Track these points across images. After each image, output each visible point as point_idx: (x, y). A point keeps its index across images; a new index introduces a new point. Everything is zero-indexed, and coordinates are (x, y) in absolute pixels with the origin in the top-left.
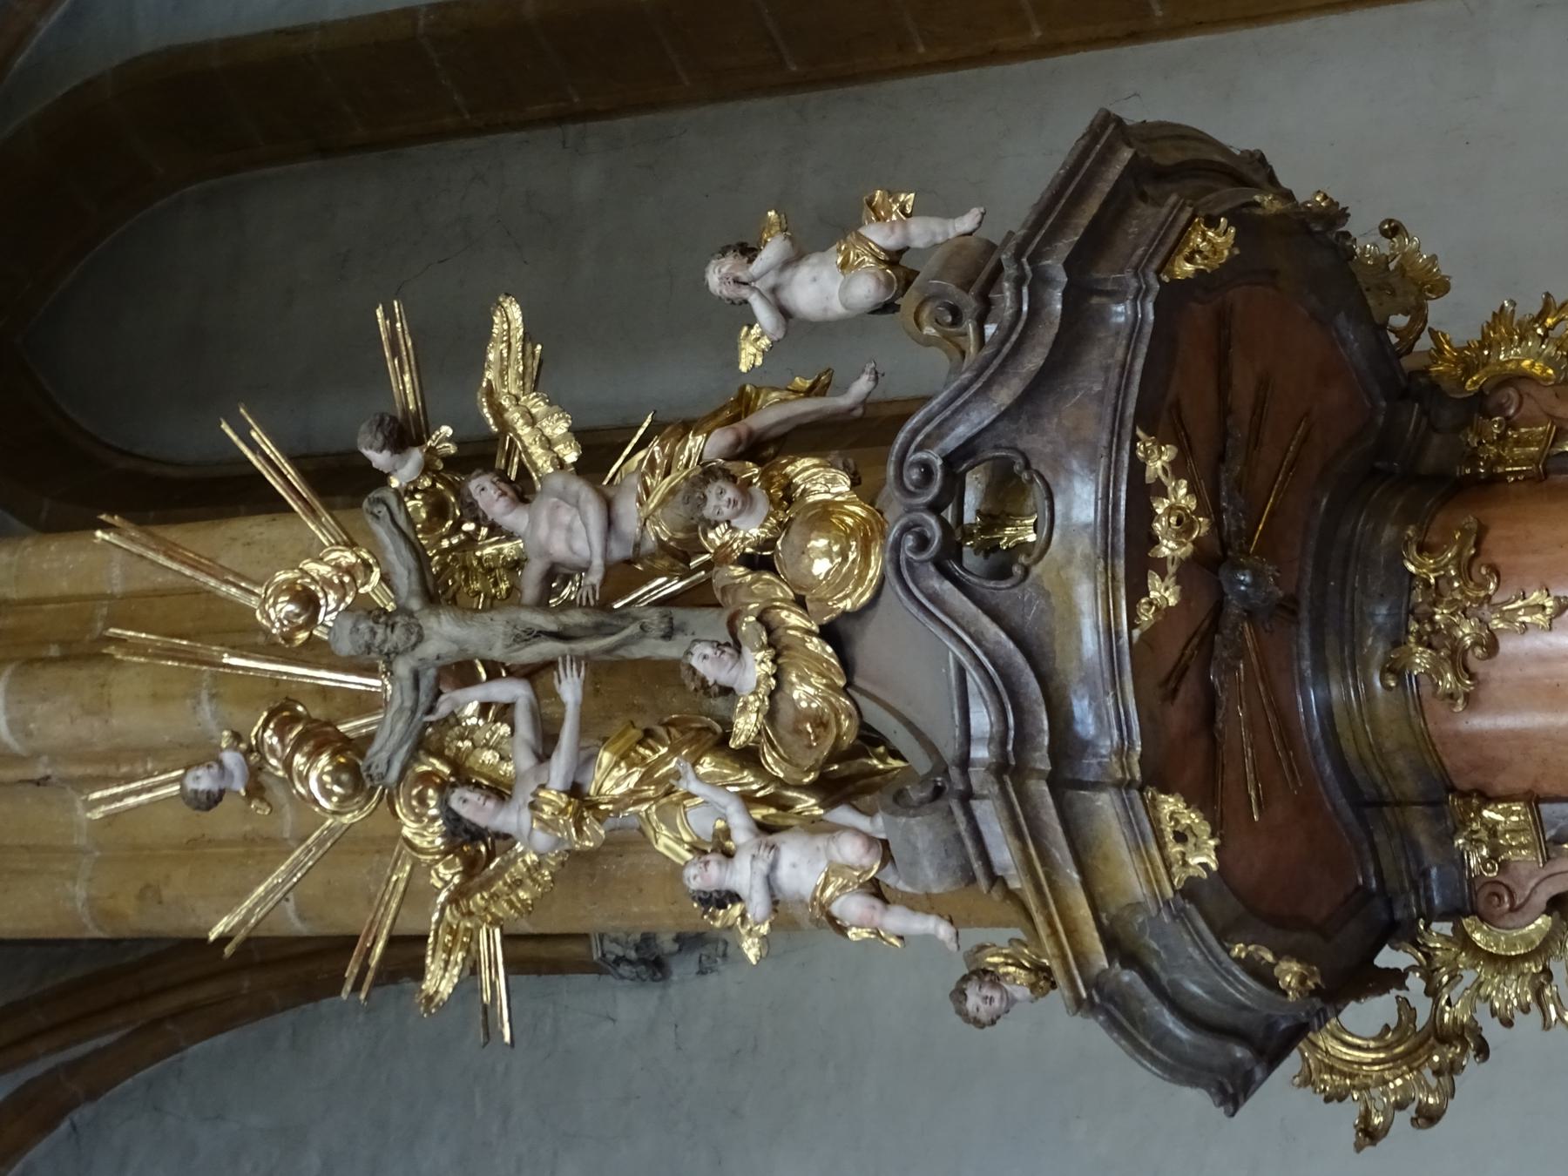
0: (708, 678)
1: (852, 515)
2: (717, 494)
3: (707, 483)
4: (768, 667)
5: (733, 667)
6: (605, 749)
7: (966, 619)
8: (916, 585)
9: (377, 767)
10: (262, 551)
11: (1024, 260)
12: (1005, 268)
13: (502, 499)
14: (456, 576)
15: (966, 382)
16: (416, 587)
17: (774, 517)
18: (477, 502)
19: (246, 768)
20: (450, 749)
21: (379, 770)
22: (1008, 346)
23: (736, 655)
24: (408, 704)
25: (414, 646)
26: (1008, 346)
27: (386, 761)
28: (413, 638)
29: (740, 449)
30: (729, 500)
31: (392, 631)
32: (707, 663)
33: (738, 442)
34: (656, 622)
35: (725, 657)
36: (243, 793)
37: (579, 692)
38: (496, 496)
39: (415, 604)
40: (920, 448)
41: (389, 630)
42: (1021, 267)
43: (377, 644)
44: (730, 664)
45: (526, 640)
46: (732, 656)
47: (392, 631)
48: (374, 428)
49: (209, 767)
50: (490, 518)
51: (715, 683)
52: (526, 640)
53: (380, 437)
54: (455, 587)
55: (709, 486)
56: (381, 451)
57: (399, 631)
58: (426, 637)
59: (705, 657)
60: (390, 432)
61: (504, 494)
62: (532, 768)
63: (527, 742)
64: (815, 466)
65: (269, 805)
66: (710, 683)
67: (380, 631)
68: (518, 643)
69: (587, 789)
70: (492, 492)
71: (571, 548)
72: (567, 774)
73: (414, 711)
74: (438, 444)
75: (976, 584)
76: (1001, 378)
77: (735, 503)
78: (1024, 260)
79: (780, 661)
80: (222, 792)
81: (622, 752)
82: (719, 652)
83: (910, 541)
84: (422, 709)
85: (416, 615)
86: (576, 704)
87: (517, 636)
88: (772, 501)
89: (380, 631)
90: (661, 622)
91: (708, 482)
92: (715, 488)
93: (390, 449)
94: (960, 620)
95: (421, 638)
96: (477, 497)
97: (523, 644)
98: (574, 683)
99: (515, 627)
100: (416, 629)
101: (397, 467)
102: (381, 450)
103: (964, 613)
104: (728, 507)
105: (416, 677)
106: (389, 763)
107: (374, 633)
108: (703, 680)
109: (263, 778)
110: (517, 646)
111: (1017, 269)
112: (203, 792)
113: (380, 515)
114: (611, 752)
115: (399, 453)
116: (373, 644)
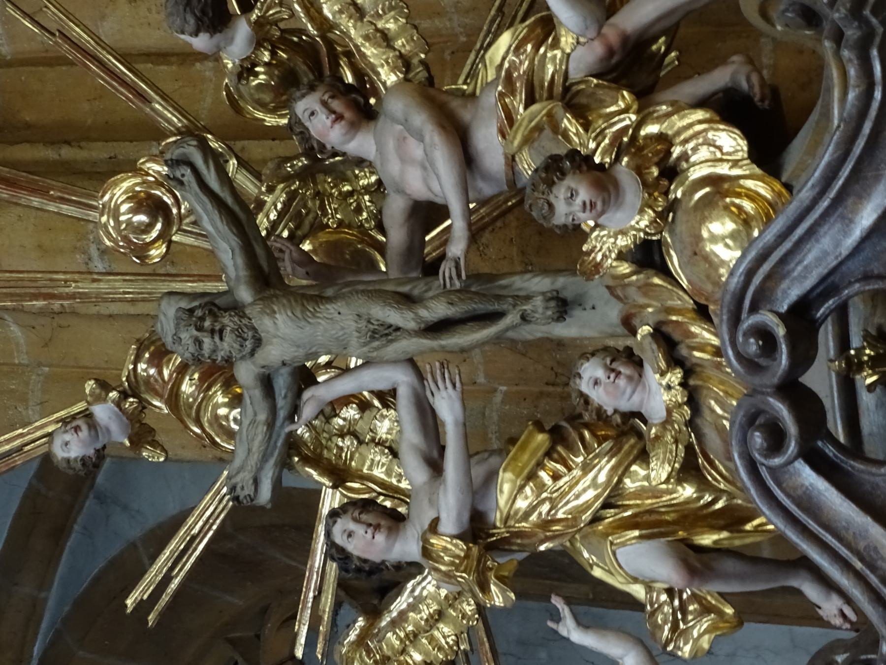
0: (605, 408)
1: (753, 196)
2: (566, 199)
3: (551, 184)
4: (679, 395)
5: (633, 392)
6: (505, 471)
7: (851, 532)
8: (779, 485)
9: (243, 488)
10: (149, 10)
11: (867, 12)
12: (844, 29)
13: (337, 126)
14: (310, 203)
15: (807, 202)
16: (243, 273)
17: (650, 207)
18: (307, 129)
19: (124, 418)
20: (329, 449)
21: (246, 492)
22: (860, 143)
23: (636, 376)
24: (262, 417)
25: (252, 353)
26: (860, 143)
27: (251, 481)
28: (249, 344)
29: (614, 60)
30: (584, 203)
31: (221, 339)
32: (600, 390)
33: (610, 52)
34: (540, 310)
35: (622, 382)
36: (127, 443)
37: (458, 406)
38: (329, 122)
39: (245, 294)
40: (754, 308)
41: (217, 339)
42: (864, 22)
43: (207, 355)
44: (629, 390)
45: (387, 335)
46: (630, 378)
47: (221, 339)
48: (181, 8)
49: (77, 429)
50: (329, 147)
51: (616, 411)
52: (387, 335)
53: (192, 21)
54: (311, 217)
55: (555, 190)
56: (197, 35)
57: (228, 337)
58: (264, 340)
59: (596, 383)
60: (203, 12)
61: (339, 118)
62: (425, 483)
63: (415, 448)
64: (700, 122)
65: (164, 450)
66: (610, 412)
67: (207, 342)
68: (378, 339)
69: (491, 517)
70: (324, 117)
71: (430, 189)
72: (459, 515)
73: (271, 424)
74: (267, 11)
75: (862, 471)
76: (857, 187)
77: (593, 205)
78: (867, 12)
79: (692, 382)
80: (101, 454)
81: (526, 472)
82: (612, 376)
83: (758, 439)
84: (282, 414)
85: (247, 311)
86: (456, 423)
87: (374, 332)
88: (645, 184)
89: (207, 342)
90: (547, 308)
91: (553, 183)
92: (563, 190)
93: (207, 31)
94: (843, 533)
95: (258, 342)
96: (307, 124)
97: (384, 340)
98: (450, 397)
99: (369, 322)
100: (250, 334)
101: (222, 45)
102: (196, 34)
103: (848, 523)
104: (584, 212)
105: (267, 383)
106: (256, 482)
107: (199, 342)
108: (600, 411)
109: (149, 420)
110: (376, 344)
111: (860, 27)
112: (76, 459)
113: (185, 179)
114: (513, 472)
115: (220, 32)
116: (203, 355)
